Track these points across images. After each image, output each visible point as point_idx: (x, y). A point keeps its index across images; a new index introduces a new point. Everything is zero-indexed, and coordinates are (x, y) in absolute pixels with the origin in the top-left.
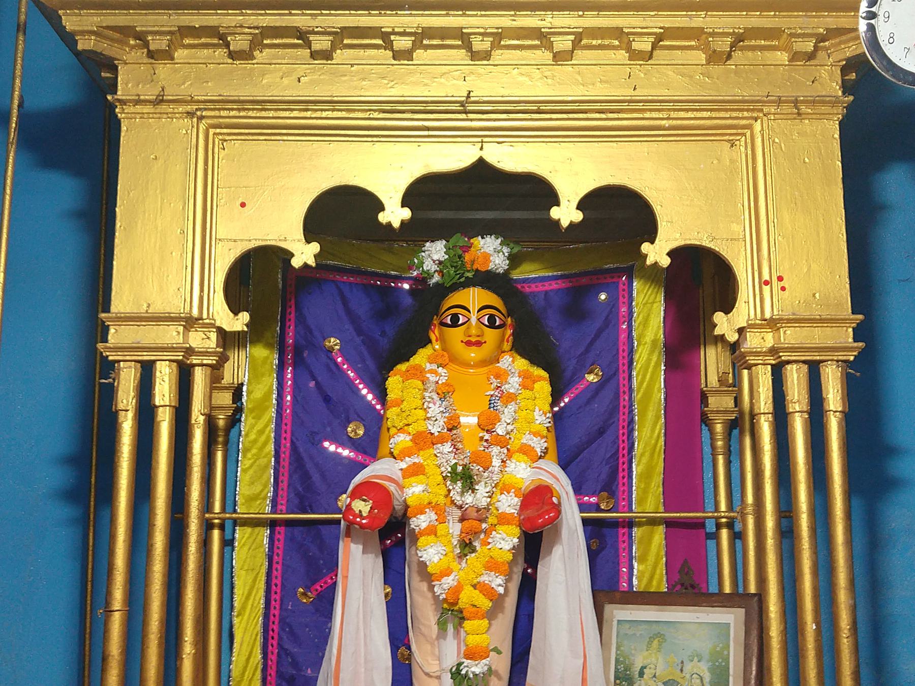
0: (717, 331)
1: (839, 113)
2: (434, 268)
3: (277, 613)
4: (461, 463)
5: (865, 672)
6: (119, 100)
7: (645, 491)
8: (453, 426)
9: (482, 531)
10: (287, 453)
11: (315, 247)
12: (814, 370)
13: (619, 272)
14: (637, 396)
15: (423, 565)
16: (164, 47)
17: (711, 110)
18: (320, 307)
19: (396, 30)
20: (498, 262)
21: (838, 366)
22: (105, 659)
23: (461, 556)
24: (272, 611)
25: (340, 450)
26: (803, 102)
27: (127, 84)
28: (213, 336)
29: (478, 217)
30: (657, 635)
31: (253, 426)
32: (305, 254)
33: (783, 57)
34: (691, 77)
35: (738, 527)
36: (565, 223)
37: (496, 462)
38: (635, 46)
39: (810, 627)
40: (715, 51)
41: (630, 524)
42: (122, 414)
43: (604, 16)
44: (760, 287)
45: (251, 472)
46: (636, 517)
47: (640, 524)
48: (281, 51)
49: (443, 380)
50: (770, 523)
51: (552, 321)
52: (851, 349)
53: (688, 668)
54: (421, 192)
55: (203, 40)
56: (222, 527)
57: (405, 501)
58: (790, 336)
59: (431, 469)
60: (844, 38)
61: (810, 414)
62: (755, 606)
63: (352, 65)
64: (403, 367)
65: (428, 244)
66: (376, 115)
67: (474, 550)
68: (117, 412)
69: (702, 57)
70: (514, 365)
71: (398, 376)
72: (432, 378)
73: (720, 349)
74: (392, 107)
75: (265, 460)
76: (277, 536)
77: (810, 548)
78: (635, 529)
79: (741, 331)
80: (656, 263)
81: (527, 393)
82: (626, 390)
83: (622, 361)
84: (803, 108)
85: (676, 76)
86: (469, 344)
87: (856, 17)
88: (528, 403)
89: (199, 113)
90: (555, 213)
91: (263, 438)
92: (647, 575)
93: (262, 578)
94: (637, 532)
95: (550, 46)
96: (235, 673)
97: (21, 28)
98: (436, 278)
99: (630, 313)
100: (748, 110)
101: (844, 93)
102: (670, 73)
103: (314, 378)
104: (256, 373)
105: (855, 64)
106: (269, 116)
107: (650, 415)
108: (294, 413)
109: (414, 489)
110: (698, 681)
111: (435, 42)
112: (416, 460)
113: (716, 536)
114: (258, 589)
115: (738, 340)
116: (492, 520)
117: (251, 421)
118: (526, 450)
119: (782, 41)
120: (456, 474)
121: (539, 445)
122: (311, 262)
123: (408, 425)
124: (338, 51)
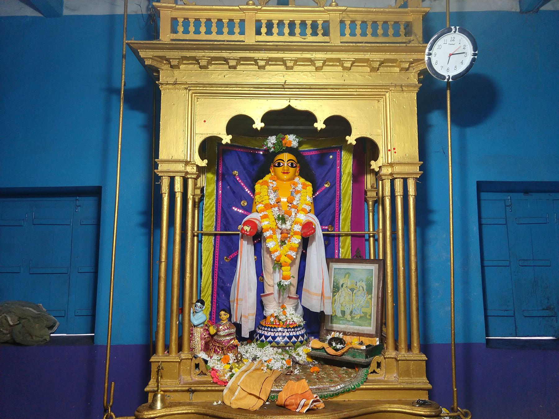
0: (372, 168)
1: (416, 90)
2: (272, 146)
6: (161, 83)
7: (345, 224)
8: (278, 202)
11: (230, 137)
12: (405, 181)
14: (342, 192)
15: (268, 249)
16: (176, 64)
18: (231, 160)
20: (295, 144)
22: (159, 278)
23: (281, 246)
27: (165, 76)
28: (195, 168)
30: (348, 273)
31: (208, 202)
32: (227, 139)
33: (397, 70)
34: (364, 77)
35: (376, 237)
36: (319, 129)
37: (293, 214)
38: (345, 65)
39: (401, 268)
41: (339, 236)
42: (164, 194)
45: (207, 217)
47: (342, 236)
48: (218, 66)
49: (275, 186)
50: (388, 233)
51: (313, 165)
53: (358, 284)
54: (269, 117)
55: (190, 62)
56: (198, 236)
58: (397, 169)
62: (382, 264)
64: (260, 181)
66: (252, 89)
67: (285, 244)
68: (162, 194)
69: (368, 69)
70: (300, 180)
72: (271, 185)
79: (380, 167)
81: (304, 190)
84: (404, 88)
85: (359, 76)
86: (284, 173)
87: (424, 55)
88: (305, 194)
91: (212, 205)
92: (344, 253)
93: (212, 255)
94: (341, 239)
95: (314, 65)
97: (124, 57)
98: (272, 150)
99: (341, 163)
103: (229, 185)
104: (209, 182)
105: (423, 73)
107: (347, 198)
111: (273, 63)
113: (368, 240)
116: (292, 233)
117: (207, 200)
118: (303, 210)
121: (308, 208)
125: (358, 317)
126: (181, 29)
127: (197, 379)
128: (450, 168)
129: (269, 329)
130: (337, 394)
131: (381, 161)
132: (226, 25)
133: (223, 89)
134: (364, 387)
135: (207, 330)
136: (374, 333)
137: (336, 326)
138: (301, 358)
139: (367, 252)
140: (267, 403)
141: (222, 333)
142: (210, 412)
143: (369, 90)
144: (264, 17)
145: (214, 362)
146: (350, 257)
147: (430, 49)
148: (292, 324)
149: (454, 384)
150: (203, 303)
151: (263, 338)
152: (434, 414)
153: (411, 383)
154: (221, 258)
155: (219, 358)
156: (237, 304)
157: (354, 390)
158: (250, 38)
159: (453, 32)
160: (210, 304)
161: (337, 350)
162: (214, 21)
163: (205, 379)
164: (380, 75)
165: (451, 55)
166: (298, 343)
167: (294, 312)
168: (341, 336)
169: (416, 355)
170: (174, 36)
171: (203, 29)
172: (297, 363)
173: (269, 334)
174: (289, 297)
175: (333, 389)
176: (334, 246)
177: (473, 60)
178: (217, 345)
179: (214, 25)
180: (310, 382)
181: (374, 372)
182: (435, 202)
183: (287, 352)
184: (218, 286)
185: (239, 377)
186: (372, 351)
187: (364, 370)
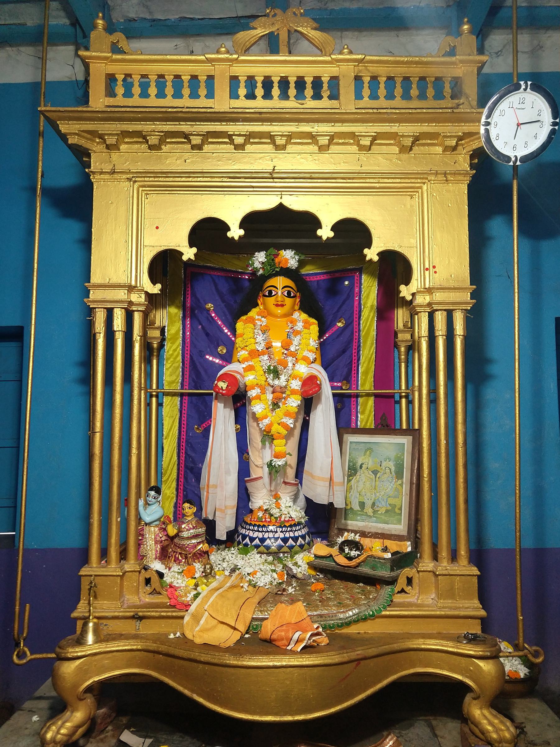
1: (467, 180)
3: (184, 437)
4: (273, 365)
5: (470, 467)
7: (365, 380)
8: (269, 347)
9: (283, 398)
10: (188, 361)
12: (450, 314)
13: (354, 270)
14: (363, 334)
15: (254, 414)
17: (401, 178)
18: (204, 288)
19: (236, 133)
21: (462, 312)
23: (273, 410)
24: (182, 437)
25: (214, 360)
26: (449, 174)
28: (143, 296)
29: (284, 242)
30: (369, 449)
31: (171, 347)
33: (439, 149)
34: (391, 160)
37: (290, 365)
38: (362, 142)
39: (443, 442)
40: (403, 146)
41: (357, 396)
42: (98, 335)
43: (346, 126)
44: (424, 272)
45: (170, 370)
46: (360, 393)
47: (362, 396)
48: (175, 146)
49: (264, 324)
51: (321, 295)
52: (469, 303)
53: (384, 464)
54: (251, 221)
55: (135, 140)
56: (157, 396)
57: (245, 383)
58: (438, 296)
59: (258, 368)
60: (472, 138)
61: (447, 336)
62: (415, 434)
63: (213, 153)
64: (244, 318)
65: (256, 253)
66: (225, 180)
67: (279, 407)
69: (396, 149)
70: (300, 317)
71: (242, 322)
72: (259, 323)
73: (404, 310)
74: (234, 176)
75: (177, 364)
76: (184, 401)
77: (444, 403)
78: (359, 399)
79: (413, 295)
80: (371, 259)
81: (306, 331)
82: (357, 331)
83: (356, 316)
84: (449, 177)
85: (384, 159)
86: (277, 305)
87: (479, 126)
89: (133, 179)
90: (319, 232)
91: (176, 353)
92: (365, 421)
94: (360, 400)
96: (164, 466)
98: (261, 272)
99: (360, 291)
100: (420, 178)
101: (471, 169)
102: (380, 158)
103: (201, 324)
104: (170, 319)
106: (169, 181)
107: (369, 343)
108: (191, 341)
109: (249, 377)
110: (389, 471)
111: (256, 140)
112: (250, 363)
113: (399, 402)
114: (175, 426)
115: (412, 300)
116: (288, 393)
117: (169, 345)
118: (305, 359)
119: (439, 140)
120: (270, 370)
122: (193, 258)
123: (246, 346)
124: (206, 146)
125: (383, 510)
126: (120, 90)
127: (148, 599)
128: (516, 295)
129: (256, 528)
130: (348, 624)
131: (415, 285)
132: (186, 84)
133: (183, 179)
134: (388, 613)
135: (165, 530)
136: (405, 533)
137: (352, 524)
138: (299, 570)
139: (397, 418)
140: (247, 636)
141: (185, 534)
142: (163, 648)
143: (398, 180)
144: (242, 71)
145: (174, 575)
146: (373, 427)
147: (488, 116)
148: (289, 520)
149: (519, 609)
150: (158, 490)
151: (247, 540)
152: (489, 654)
153: (456, 608)
154: (189, 428)
155: (181, 571)
156: (208, 492)
157: (373, 617)
158: (222, 102)
159: (522, 89)
160: (175, 492)
161: (350, 559)
162: (169, 78)
163: (159, 601)
164: (415, 158)
165: (519, 125)
166: (297, 548)
167: (291, 504)
168: (357, 538)
169: (466, 568)
170: (111, 101)
171: (153, 91)
172: (294, 576)
173: (256, 534)
174: (285, 483)
175: (342, 616)
176: (350, 411)
177: (553, 132)
178: (179, 550)
179: (169, 84)
180: (309, 605)
181: (403, 591)
182: (494, 349)
183: (280, 560)
184: (186, 467)
185: (207, 597)
186: (401, 561)
187: (388, 589)
